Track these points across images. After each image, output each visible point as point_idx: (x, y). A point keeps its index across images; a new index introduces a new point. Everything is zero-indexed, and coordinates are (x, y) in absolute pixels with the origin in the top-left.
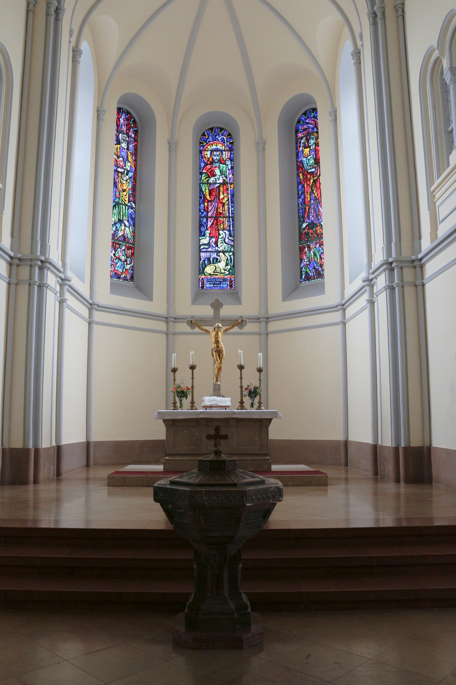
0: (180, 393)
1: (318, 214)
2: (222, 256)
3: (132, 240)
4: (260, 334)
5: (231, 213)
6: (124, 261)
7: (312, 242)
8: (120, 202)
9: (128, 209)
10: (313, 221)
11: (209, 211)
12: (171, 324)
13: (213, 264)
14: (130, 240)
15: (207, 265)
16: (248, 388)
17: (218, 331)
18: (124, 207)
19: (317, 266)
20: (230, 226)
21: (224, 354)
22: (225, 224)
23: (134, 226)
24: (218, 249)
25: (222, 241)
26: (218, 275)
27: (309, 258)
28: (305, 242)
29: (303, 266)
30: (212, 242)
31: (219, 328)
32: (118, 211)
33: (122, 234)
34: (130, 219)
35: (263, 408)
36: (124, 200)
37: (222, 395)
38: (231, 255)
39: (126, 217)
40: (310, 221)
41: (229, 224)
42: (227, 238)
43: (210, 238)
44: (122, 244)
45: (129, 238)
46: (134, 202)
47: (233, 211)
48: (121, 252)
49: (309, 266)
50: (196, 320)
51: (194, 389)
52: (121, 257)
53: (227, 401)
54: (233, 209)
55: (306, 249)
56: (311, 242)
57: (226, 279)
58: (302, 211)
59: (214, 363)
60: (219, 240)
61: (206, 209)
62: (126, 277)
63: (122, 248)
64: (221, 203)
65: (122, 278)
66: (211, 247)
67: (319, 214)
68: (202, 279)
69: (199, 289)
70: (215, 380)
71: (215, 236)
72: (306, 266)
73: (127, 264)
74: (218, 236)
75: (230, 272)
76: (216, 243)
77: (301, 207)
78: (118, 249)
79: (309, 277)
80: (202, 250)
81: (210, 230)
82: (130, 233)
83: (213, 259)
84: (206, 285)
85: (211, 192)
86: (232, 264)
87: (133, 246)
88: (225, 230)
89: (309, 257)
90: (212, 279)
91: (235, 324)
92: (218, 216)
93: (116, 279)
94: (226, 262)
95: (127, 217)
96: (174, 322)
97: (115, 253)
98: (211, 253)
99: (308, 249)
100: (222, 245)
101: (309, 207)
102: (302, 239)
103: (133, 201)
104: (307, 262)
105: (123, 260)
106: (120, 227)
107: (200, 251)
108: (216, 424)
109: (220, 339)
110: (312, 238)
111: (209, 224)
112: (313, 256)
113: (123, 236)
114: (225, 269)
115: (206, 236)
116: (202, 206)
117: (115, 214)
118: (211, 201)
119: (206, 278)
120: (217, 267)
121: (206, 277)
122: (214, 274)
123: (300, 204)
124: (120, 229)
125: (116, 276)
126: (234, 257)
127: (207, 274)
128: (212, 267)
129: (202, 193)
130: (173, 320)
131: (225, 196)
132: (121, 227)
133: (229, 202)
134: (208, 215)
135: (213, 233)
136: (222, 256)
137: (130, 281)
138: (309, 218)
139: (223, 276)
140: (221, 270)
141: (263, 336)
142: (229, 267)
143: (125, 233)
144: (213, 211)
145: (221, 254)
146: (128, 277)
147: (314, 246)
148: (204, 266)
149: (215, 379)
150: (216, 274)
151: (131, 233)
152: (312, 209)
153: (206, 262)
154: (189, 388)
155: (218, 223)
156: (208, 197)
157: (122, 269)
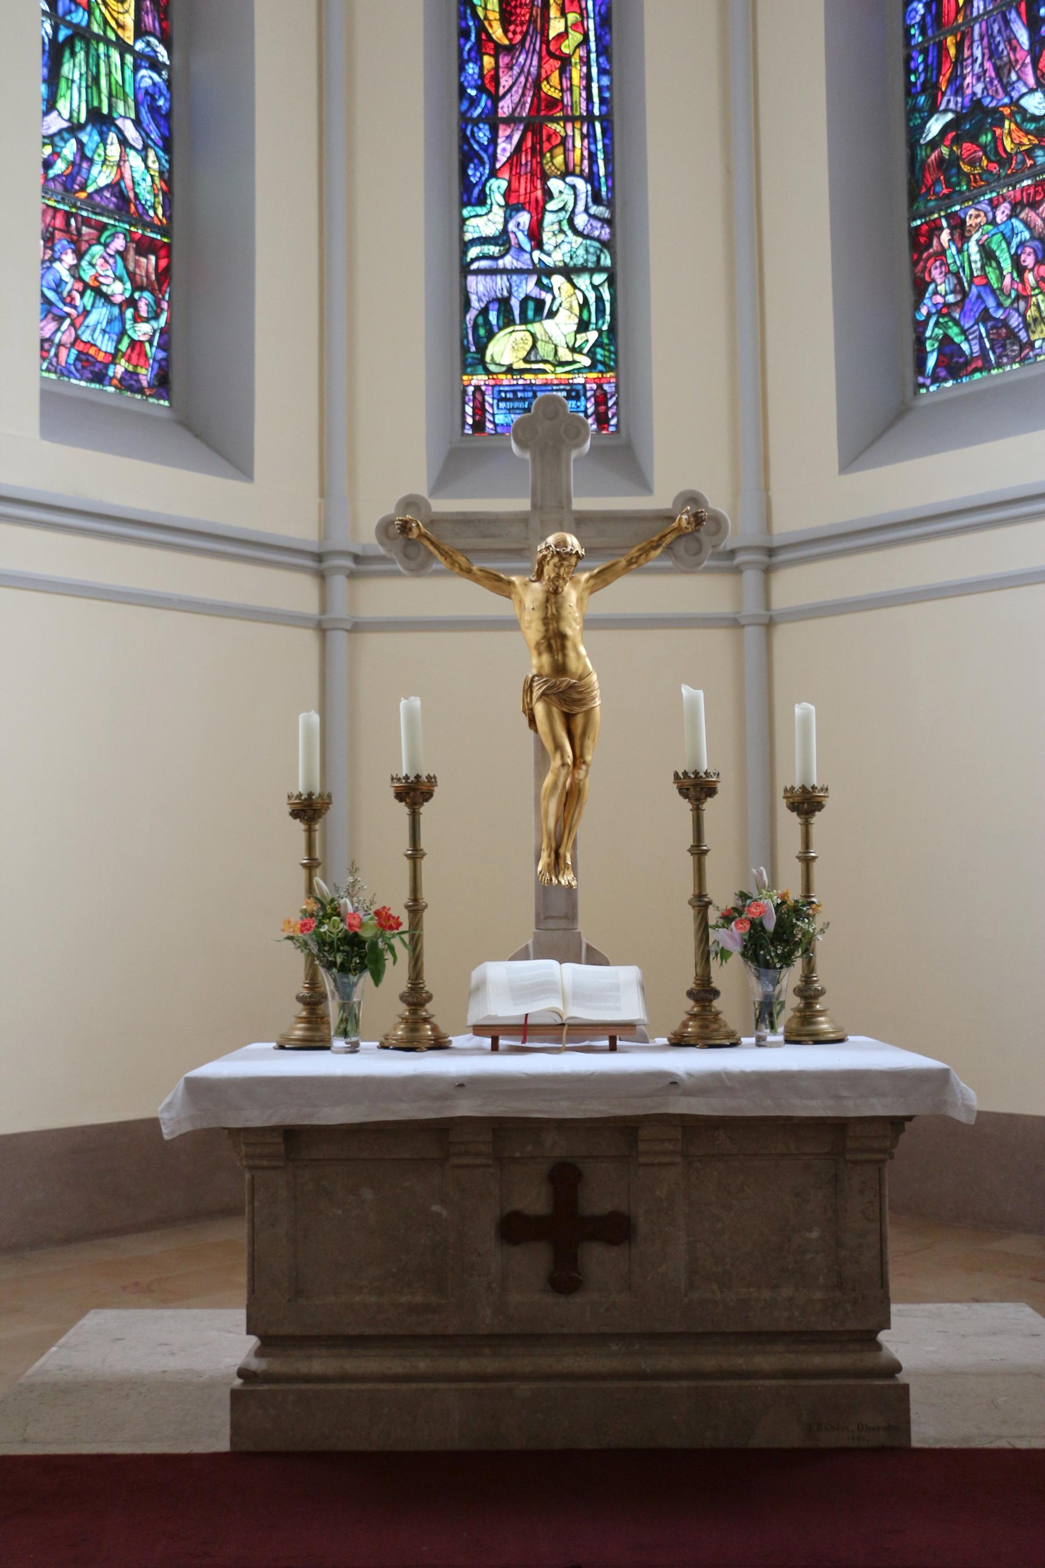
0: (339, 950)
1: (1005, 59)
2: (559, 288)
3: (160, 211)
4: (735, 623)
5: (596, 99)
6: (120, 305)
7: (976, 197)
8: (96, 28)
9: (136, 69)
10: (979, 101)
11: (502, 91)
12: (339, 583)
13: (521, 323)
14: (147, 211)
15: (496, 329)
16: (740, 913)
17: (558, 576)
18: (115, 55)
19: (999, 305)
20: (592, 158)
21: (598, 709)
22: (574, 146)
23: (167, 145)
24: (544, 258)
25: (560, 222)
26: (544, 372)
27: (957, 275)
28: (941, 202)
29: (929, 315)
30: (515, 230)
31: (562, 555)
32: (87, 73)
33: (109, 181)
34: (145, 117)
35: (825, 1026)
36: (113, 24)
37: (589, 948)
38: (601, 285)
39: (125, 102)
40: (967, 100)
41: (589, 149)
42: (583, 208)
43: (508, 212)
44: (109, 224)
45: (146, 201)
46: (166, 40)
47: (605, 89)
48: (106, 261)
49: (958, 310)
50: (433, 522)
51: (427, 916)
52: (108, 285)
53: (616, 988)
54: (605, 81)
55: (945, 236)
56: (968, 200)
57: (580, 387)
58: (925, 60)
59: (537, 764)
60: (549, 218)
61: (488, 86)
62: (135, 377)
63: (110, 243)
64: (551, 55)
65: (115, 382)
66: (512, 251)
67: (1010, 61)
68: (474, 393)
69: (463, 434)
70: (549, 865)
71: (529, 202)
72: (945, 311)
73: (137, 318)
74: (541, 203)
75: (599, 357)
76: (535, 235)
77: (918, 44)
78: (90, 246)
79: (962, 360)
80: (474, 266)
81: (507, 177)
82: (149, 179)
83: (524, 303)
84: (493, 415)
85: (509, 9)
86: (603, 323)
87: (165, 240)
88: (573, 174)
89: (958, 272)
90: (520, 391)
91: (656, 538)
92: (542, 113)
93: (83, 383)
94: (578, 314)
95: (132, 104)
96: (352, 575)
97: (75, 262)
98: (515, 278)
99: (951, 234)
100: (559, 241)
101: (958, 39)
102: (924, 191)
103: (158, 34)
104: (946, 294)
105: (118, 299)
106: (101, 145)
107: (465, 270)
108: (556, 1147)
109: (570, 627)
110: (976, 181)
111: (505, 149)
112: (979, 265)
113: (116, 189)
114: (576, 346)
115: (492, 204)
116: (471, 71)
117: (73, 81)
118: (510, 50)
119: (493, 386)
120: (539, 336)
121: (492, 382)
122: (528, 366)
123: (913, 31)
124: (99, 155)
125: (83, 367)
126: (615, 291)
127: (499, 367)
128: (519, 339)
129: (468, 11)
130: (349, 563)
131: (569, 24)
132: (105, 149)
133: (589, 52)
134: (497, 112)
135: (522, 191)
136: (559, 288)
137: (151, 396)
138: (959, 91)
139: (570, 376)
140: (560, 349)
141: (752, 634)
142: (592, 336)
143: (122, 177)
144: (520, 91)
145: (557, 280)
146: (146, 375)
147: (986, 215)
148: (482, 332)
149: (544, 855)
150: (534, 366)
151: (153, 181)
152: (975, 45)
153: (493, 317)
154: (394, 913)
155: (541, 143)
156: (497, 32)
157: (115, 337)
